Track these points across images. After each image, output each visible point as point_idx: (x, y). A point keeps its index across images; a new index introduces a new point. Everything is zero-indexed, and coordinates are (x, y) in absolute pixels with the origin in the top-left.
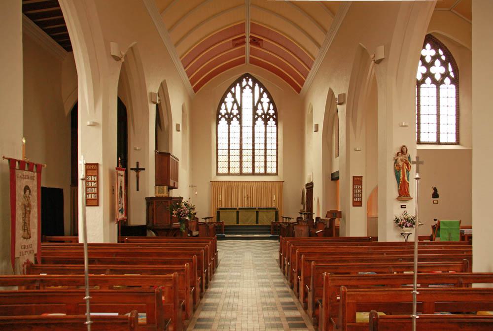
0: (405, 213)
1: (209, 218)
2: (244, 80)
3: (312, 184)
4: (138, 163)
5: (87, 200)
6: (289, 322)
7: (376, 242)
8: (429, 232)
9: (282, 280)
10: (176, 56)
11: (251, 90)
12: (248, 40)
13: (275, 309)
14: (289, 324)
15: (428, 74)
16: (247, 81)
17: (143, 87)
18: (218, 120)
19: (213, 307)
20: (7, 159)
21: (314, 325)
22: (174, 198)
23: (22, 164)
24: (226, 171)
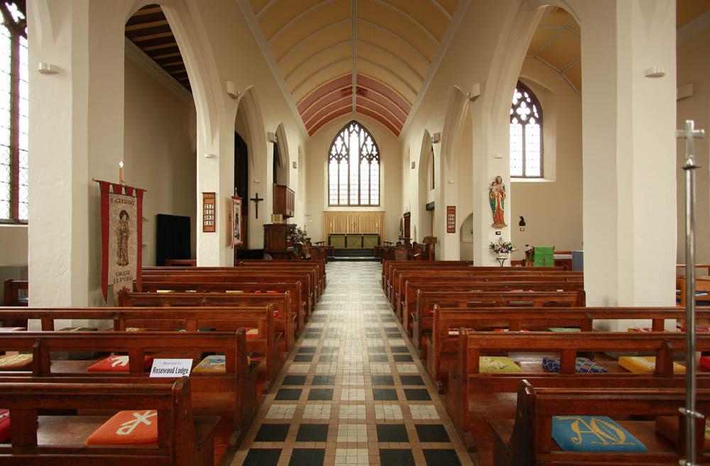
0: (501, 239)
1: (321, 243)
2: (352, 126)
3: (409, 213)
4: (257, 194)
5: (204, 227)
6: (394, 354)
7: (582, 308)
8: (523, 257)
9: (384, 303)
10: (293, 102)
11: (357, 135)
12: (354, 90)
13: (379, 336)
14: (394, 356)
15: (515, 115)
16: (354, 126)
17: (261, 128)
18: (329, 160)
19: (321, 318)
20: (98, 181)
21: (421, 359)
22: (289, 225)
23: (118, 189)
24: (336, 203)
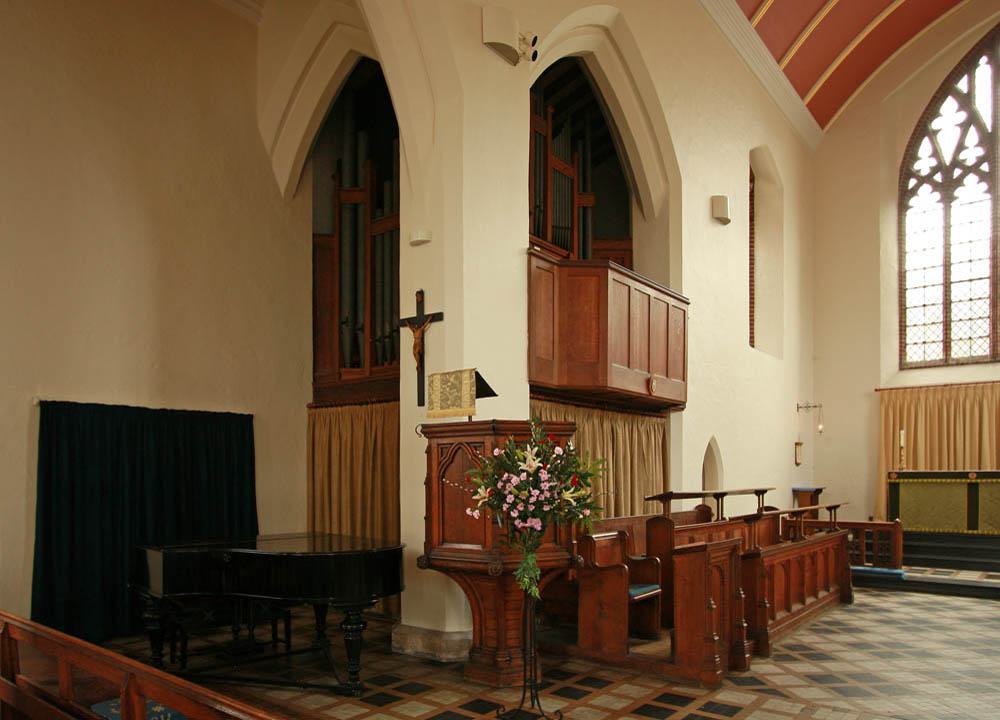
18: (904, 196)
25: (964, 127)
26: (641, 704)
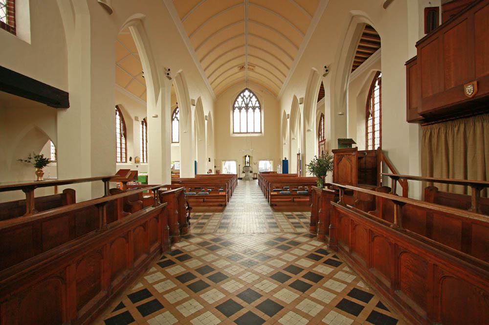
25: (242, 102)
26: (319, 248)
